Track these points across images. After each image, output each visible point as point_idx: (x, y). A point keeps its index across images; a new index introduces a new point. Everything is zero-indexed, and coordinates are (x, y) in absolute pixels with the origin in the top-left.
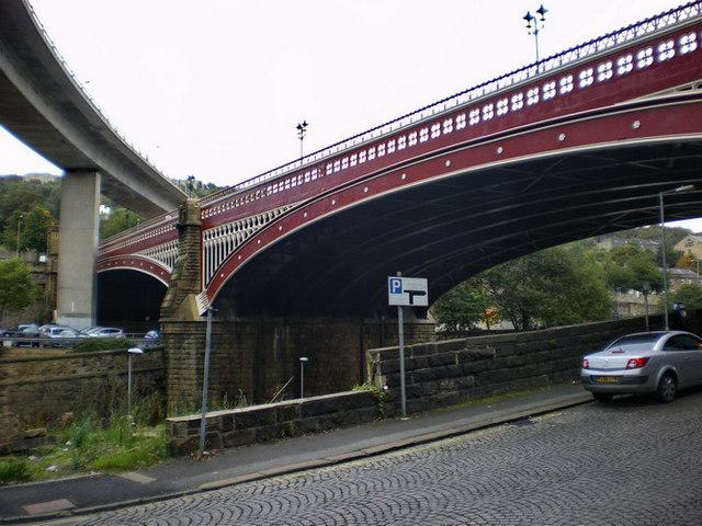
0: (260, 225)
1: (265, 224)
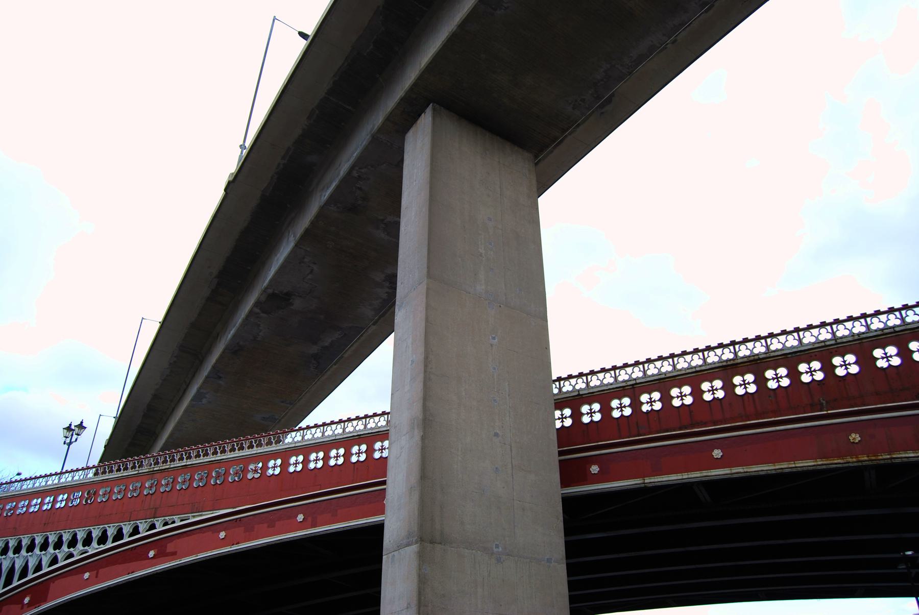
0: (94, 548)
1: (109, 544)
